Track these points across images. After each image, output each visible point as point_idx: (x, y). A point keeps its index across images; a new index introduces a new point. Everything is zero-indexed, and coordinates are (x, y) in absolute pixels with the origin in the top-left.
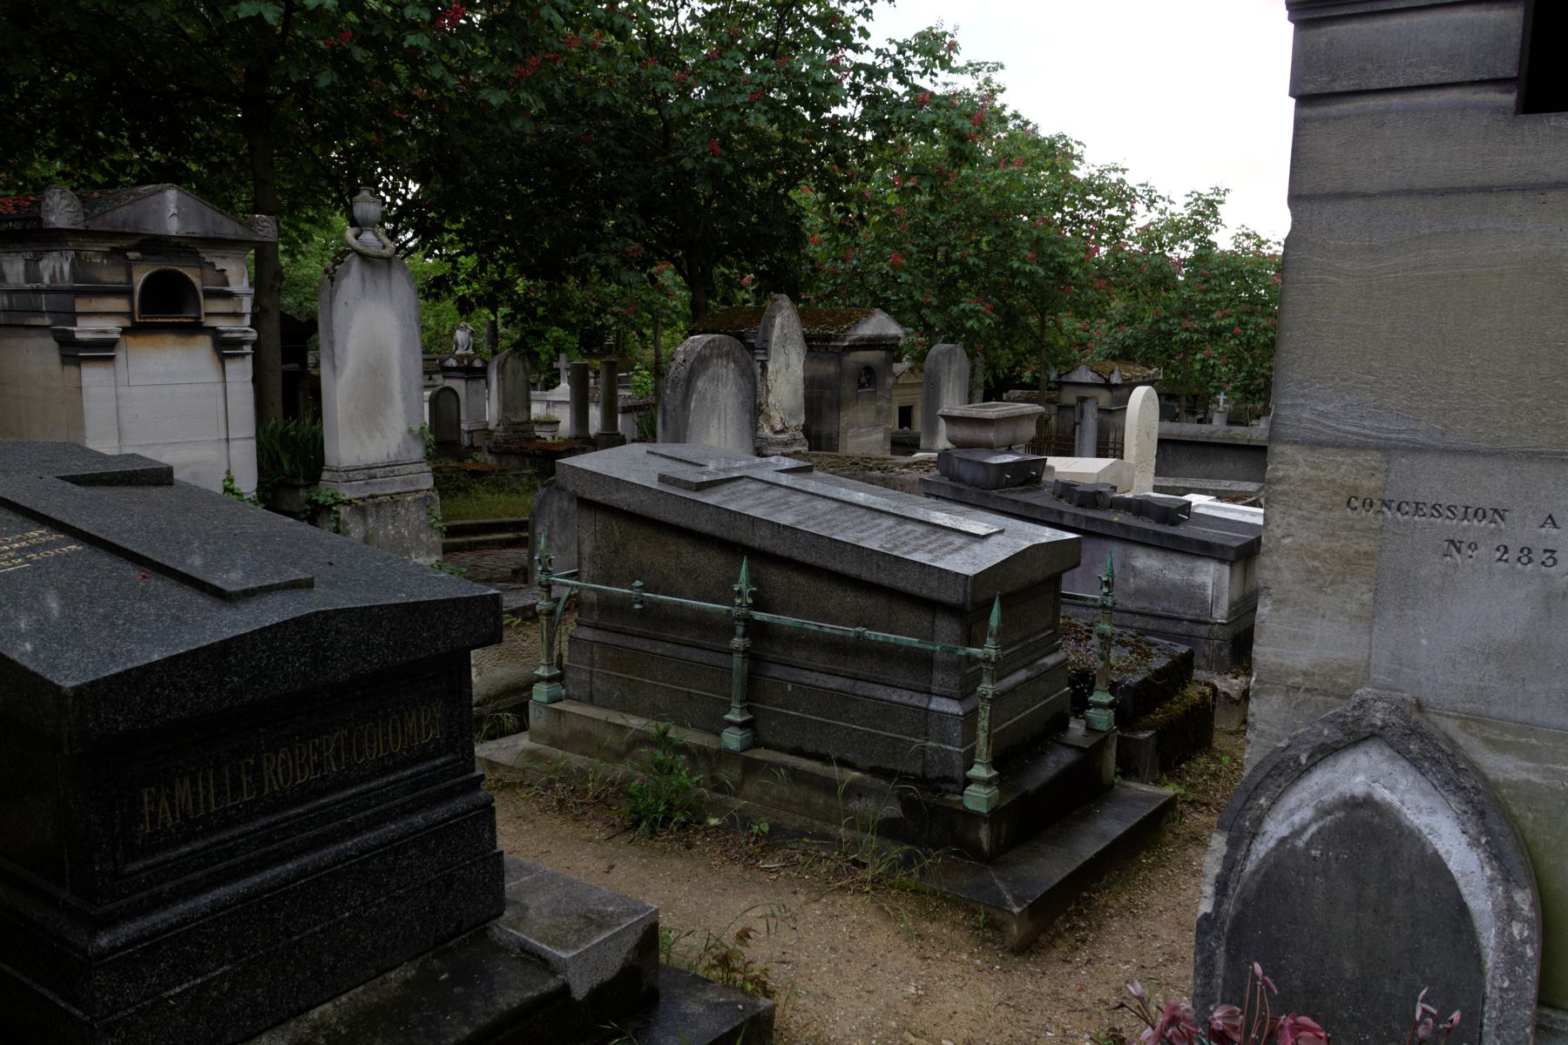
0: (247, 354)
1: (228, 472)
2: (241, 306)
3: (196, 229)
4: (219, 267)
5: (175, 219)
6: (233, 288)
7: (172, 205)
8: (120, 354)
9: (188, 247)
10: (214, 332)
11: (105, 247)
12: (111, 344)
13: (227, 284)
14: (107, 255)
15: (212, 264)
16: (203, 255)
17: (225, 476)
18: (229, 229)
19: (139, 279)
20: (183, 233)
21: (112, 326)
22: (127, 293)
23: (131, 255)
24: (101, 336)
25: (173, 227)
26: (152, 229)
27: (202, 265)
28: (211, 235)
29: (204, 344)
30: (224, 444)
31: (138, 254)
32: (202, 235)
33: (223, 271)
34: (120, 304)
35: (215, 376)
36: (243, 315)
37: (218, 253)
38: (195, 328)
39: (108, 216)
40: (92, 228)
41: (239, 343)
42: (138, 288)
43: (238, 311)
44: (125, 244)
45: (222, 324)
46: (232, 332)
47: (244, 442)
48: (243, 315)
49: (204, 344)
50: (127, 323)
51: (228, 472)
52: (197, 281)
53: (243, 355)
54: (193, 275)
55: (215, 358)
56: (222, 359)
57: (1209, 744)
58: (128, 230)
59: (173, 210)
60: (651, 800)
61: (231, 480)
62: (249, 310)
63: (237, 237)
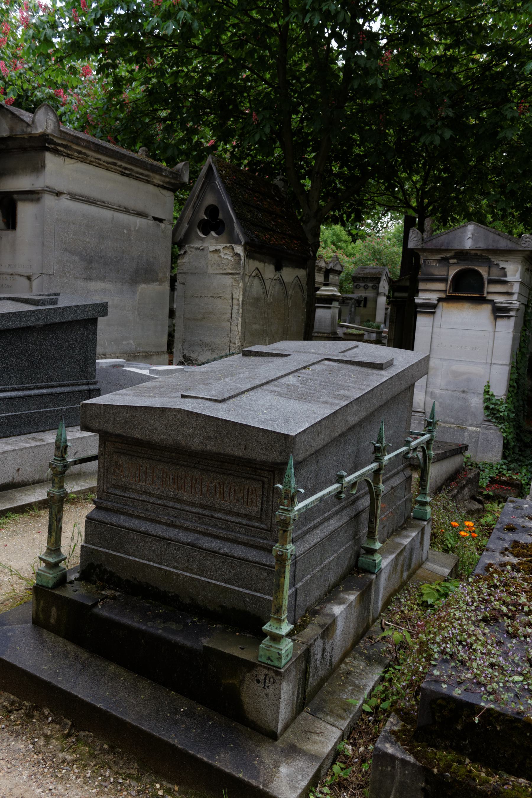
0: (512, 316)
1: (488, 382)
2: (512, 288)
3: (482, 245)
4: (501, 266)
5: (470, 240)
6: (508, 279)
7: (469, 233)
8: (438, 311)
9: (482, 256)
10: (492, 302)
11: (438, 257)
12: (434, 306)
13: (505, 276)
14: (439, 261)
15: (498, 265)
16: (493, 260)
17: (486, 384)
18: (503, 244)
19: (452, 273)
20: (474, 247)
21: (434, 297)
22: (443, 280)
23: (451, 261)
24: (427, 301)
25: (468, 244)
26: (457, 246)
27: (490, 265)
28: (490, 248)
29: (487, 309)
30: (489, 366)
31: (455, 261)
32: (485, 248)
33: (504, 269)
34: (441, 286)
35: (490, 328)
36: (513, 294)
37: (502, 258)
38: (481, 300)
39: (434, 241)
40: (425, 247)
41: (508, 310)
42: (450, 278)
43: (510, 291)
44: (449, 255)
45: (497, 298)
46: (502, 303)
47: (501, 367)
48: (513, 294)
49: (487, 309)
50: (443, 295)
51: (488, 382)
52: (485, 274)
53: (509, 317)
54: (483, 271)
55: (492, 318)
56: (496, 318)
57: (478, 53)
58: (443, 247)
59: (469, 235)
60: (526, 566)
61: (489, 387)
62: (517, 291)
63: (508, 248)
